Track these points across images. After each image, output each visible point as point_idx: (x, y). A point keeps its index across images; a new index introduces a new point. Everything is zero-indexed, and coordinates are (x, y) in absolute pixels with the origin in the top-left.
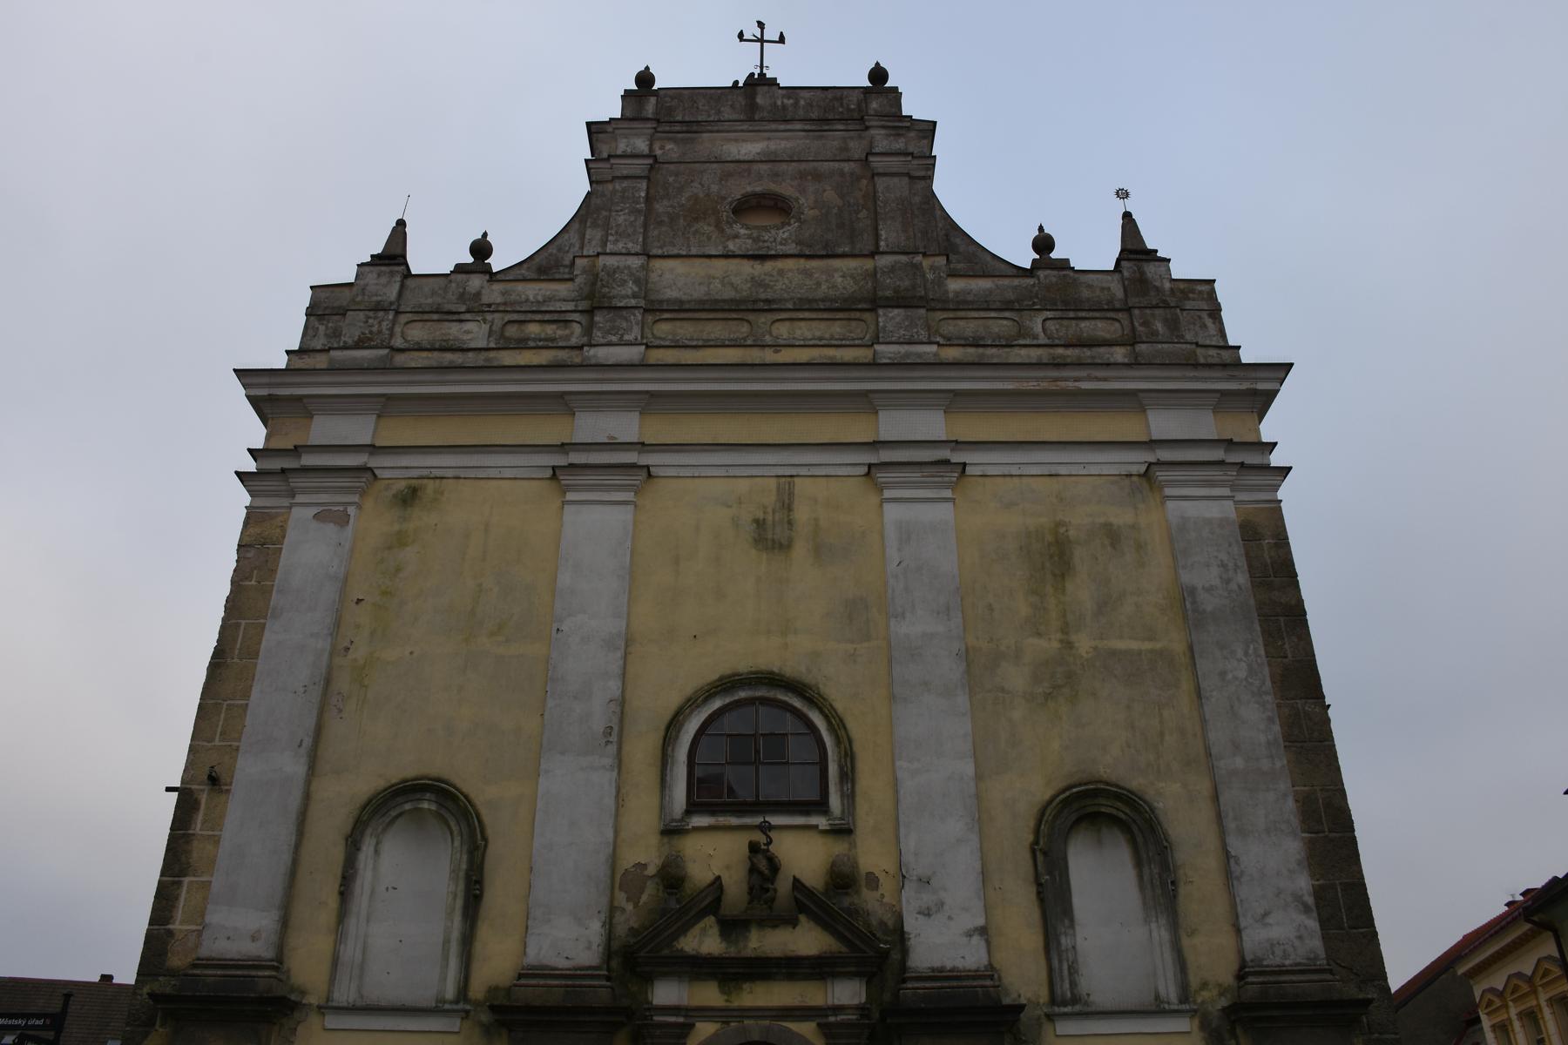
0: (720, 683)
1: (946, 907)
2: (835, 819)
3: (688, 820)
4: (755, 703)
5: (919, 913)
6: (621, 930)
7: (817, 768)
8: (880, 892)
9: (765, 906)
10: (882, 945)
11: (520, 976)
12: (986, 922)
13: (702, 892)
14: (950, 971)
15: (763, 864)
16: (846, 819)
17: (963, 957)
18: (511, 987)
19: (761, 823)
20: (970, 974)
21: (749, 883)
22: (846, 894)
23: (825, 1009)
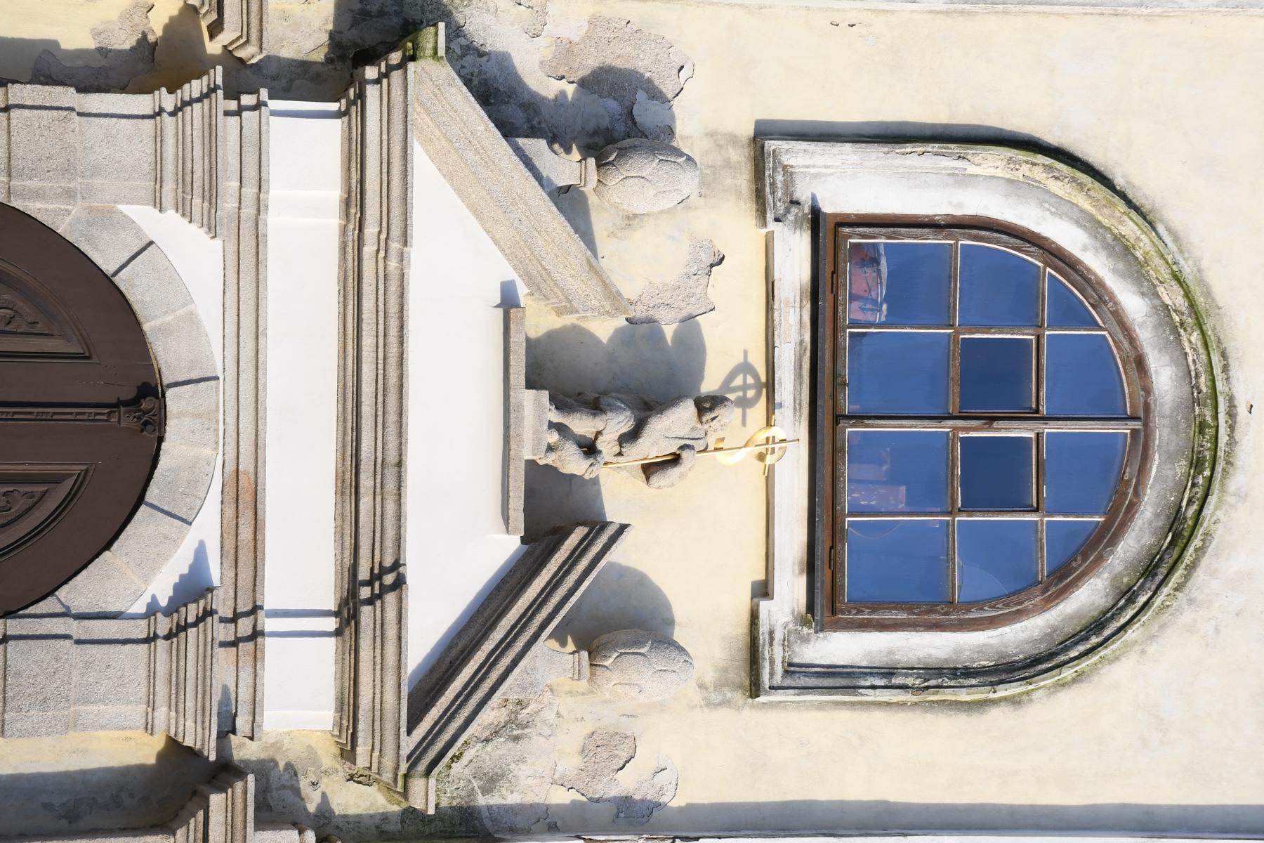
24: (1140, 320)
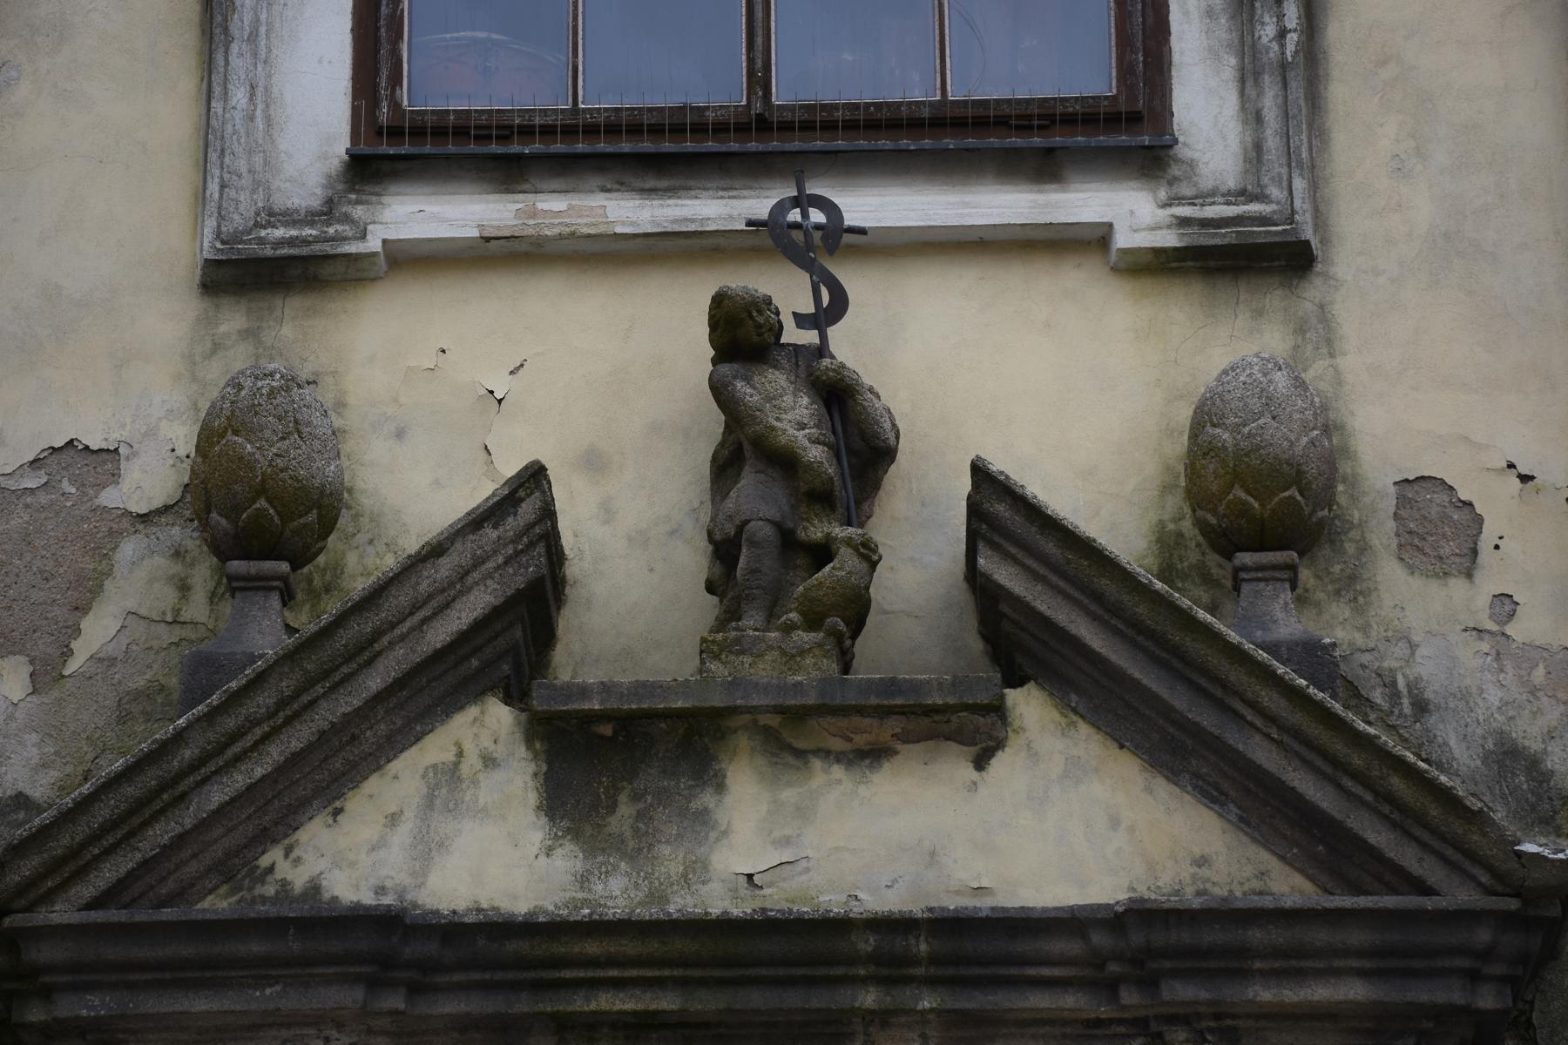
3: (358, 212)
8: (1490, 582)
9: (803, 637)
13: (435, 551)
16: (1275, 192)
19: (780, 208)
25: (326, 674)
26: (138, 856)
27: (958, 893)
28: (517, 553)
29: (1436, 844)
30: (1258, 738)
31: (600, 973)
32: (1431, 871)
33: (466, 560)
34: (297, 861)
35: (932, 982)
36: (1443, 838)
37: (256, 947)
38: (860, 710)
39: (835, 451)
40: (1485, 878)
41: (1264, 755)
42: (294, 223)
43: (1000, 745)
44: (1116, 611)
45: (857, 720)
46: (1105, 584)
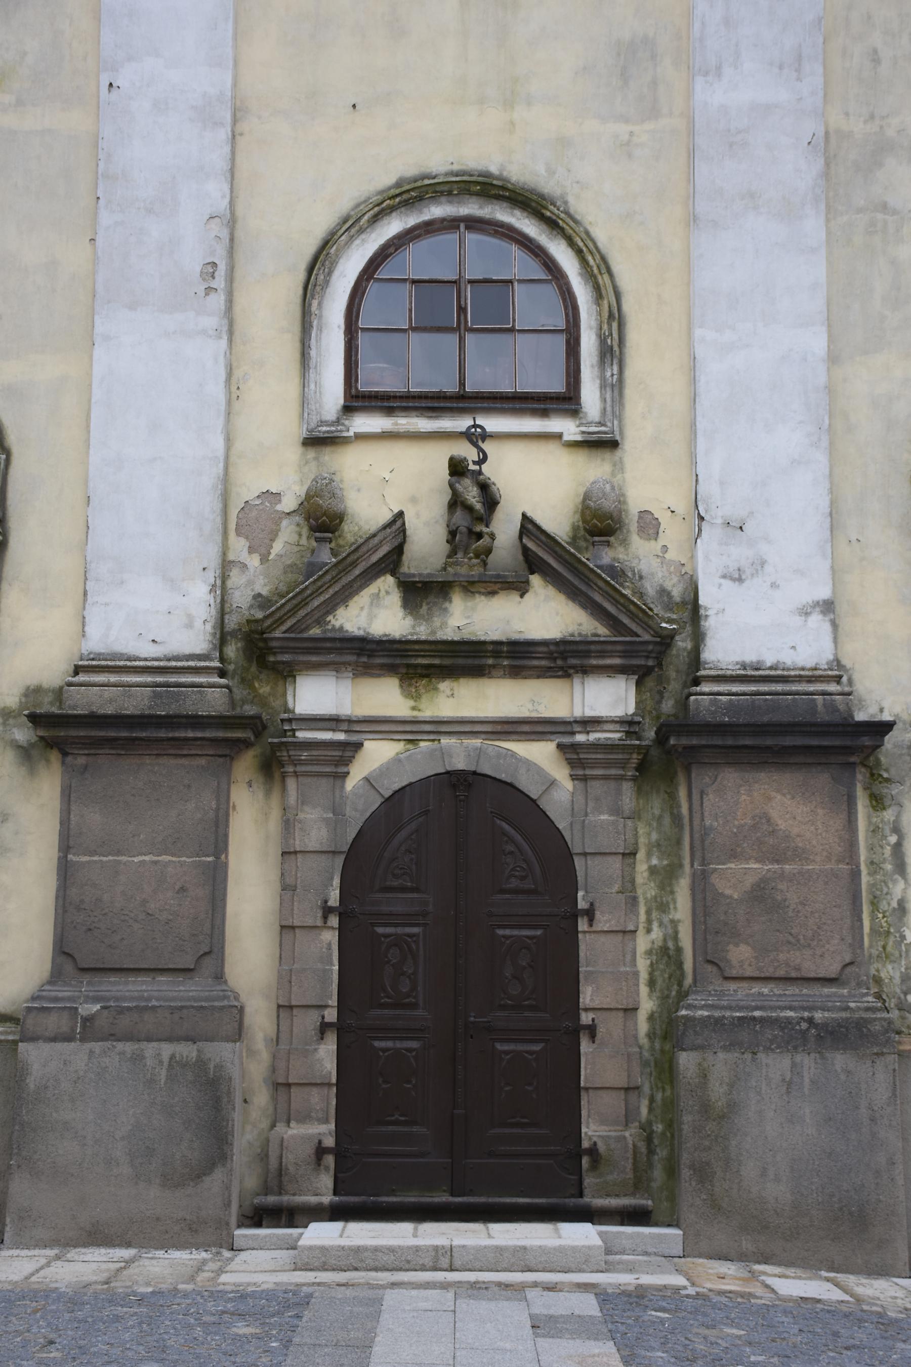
0: (398, 191)
1: (768, 568)
2: (589, 424)
3: (347, 422)
4: (458, 228)
5: (724, 577)
6: (241, 598)
7: (561, 340)
8: (662, 541)
9: (475, 561)
10: (664, 625)
11: (77, 670)
12: (834, 591)
14: (771, 668)
15: (472, 495)
16: (609, 424)
17: (793, 647)
18: (61, 688)
19: (469, 428)
20: (802, 673)
21: (448, 526)
22: (608, 544)
23: (570, 723)
24: (404, 224)
25: (344, 570)
26: (297, 619)
27: (515, 632)
28: (396, 536)
29: (640, 623)
30: (596, 593)
31: (418, 653)
32: (639, 631)
33: (382, 538)
34: (337, 619)
35: (507, 657)
36: (642, 622)
37: (328, 645)
38: (490, 582)
39: (484, 504)
40: (652, 633)
41: (598, 598)
42: (327, 425)
43: (527, 591)
44: (560, 556)
45: (488, 584)
46: (557, 549)
